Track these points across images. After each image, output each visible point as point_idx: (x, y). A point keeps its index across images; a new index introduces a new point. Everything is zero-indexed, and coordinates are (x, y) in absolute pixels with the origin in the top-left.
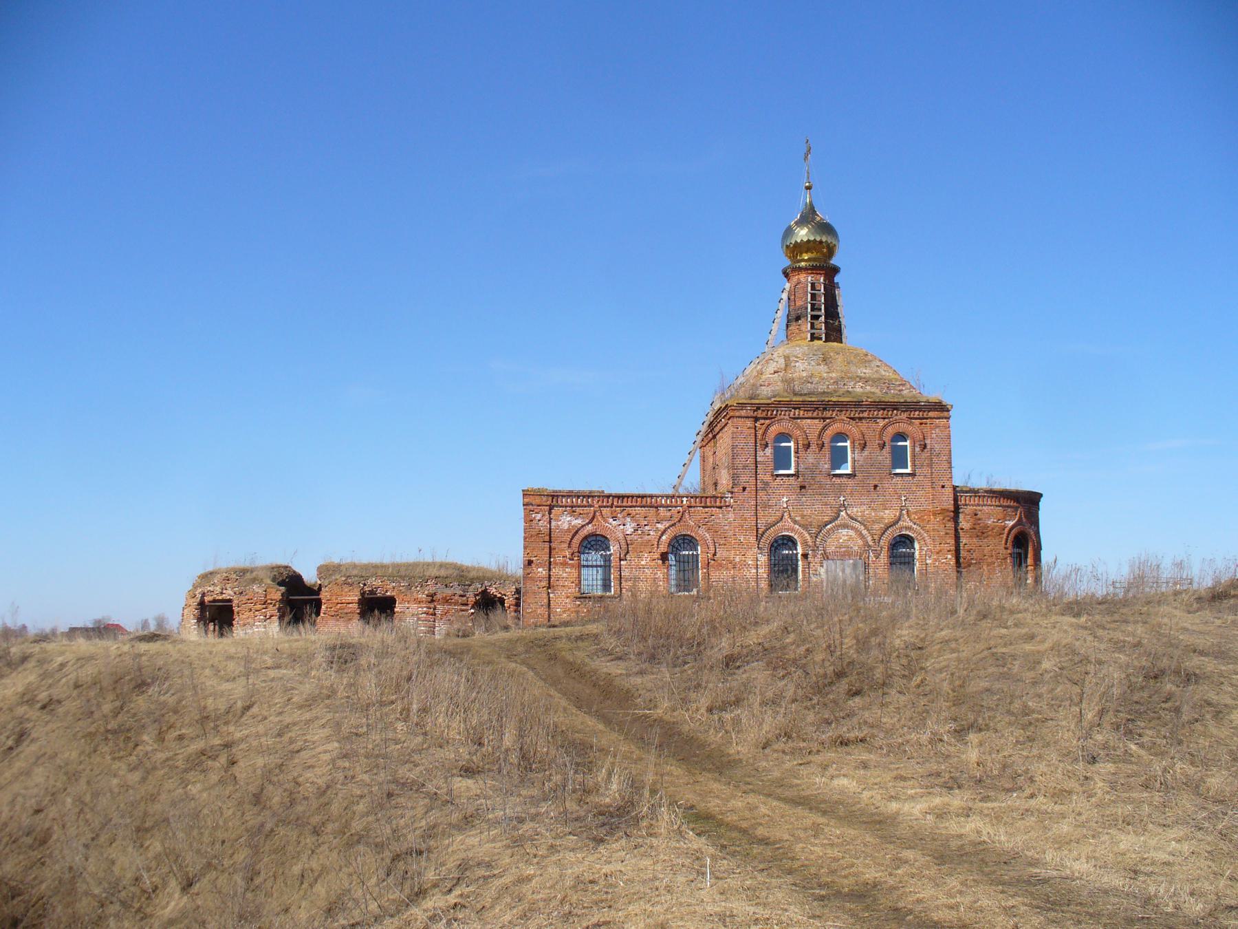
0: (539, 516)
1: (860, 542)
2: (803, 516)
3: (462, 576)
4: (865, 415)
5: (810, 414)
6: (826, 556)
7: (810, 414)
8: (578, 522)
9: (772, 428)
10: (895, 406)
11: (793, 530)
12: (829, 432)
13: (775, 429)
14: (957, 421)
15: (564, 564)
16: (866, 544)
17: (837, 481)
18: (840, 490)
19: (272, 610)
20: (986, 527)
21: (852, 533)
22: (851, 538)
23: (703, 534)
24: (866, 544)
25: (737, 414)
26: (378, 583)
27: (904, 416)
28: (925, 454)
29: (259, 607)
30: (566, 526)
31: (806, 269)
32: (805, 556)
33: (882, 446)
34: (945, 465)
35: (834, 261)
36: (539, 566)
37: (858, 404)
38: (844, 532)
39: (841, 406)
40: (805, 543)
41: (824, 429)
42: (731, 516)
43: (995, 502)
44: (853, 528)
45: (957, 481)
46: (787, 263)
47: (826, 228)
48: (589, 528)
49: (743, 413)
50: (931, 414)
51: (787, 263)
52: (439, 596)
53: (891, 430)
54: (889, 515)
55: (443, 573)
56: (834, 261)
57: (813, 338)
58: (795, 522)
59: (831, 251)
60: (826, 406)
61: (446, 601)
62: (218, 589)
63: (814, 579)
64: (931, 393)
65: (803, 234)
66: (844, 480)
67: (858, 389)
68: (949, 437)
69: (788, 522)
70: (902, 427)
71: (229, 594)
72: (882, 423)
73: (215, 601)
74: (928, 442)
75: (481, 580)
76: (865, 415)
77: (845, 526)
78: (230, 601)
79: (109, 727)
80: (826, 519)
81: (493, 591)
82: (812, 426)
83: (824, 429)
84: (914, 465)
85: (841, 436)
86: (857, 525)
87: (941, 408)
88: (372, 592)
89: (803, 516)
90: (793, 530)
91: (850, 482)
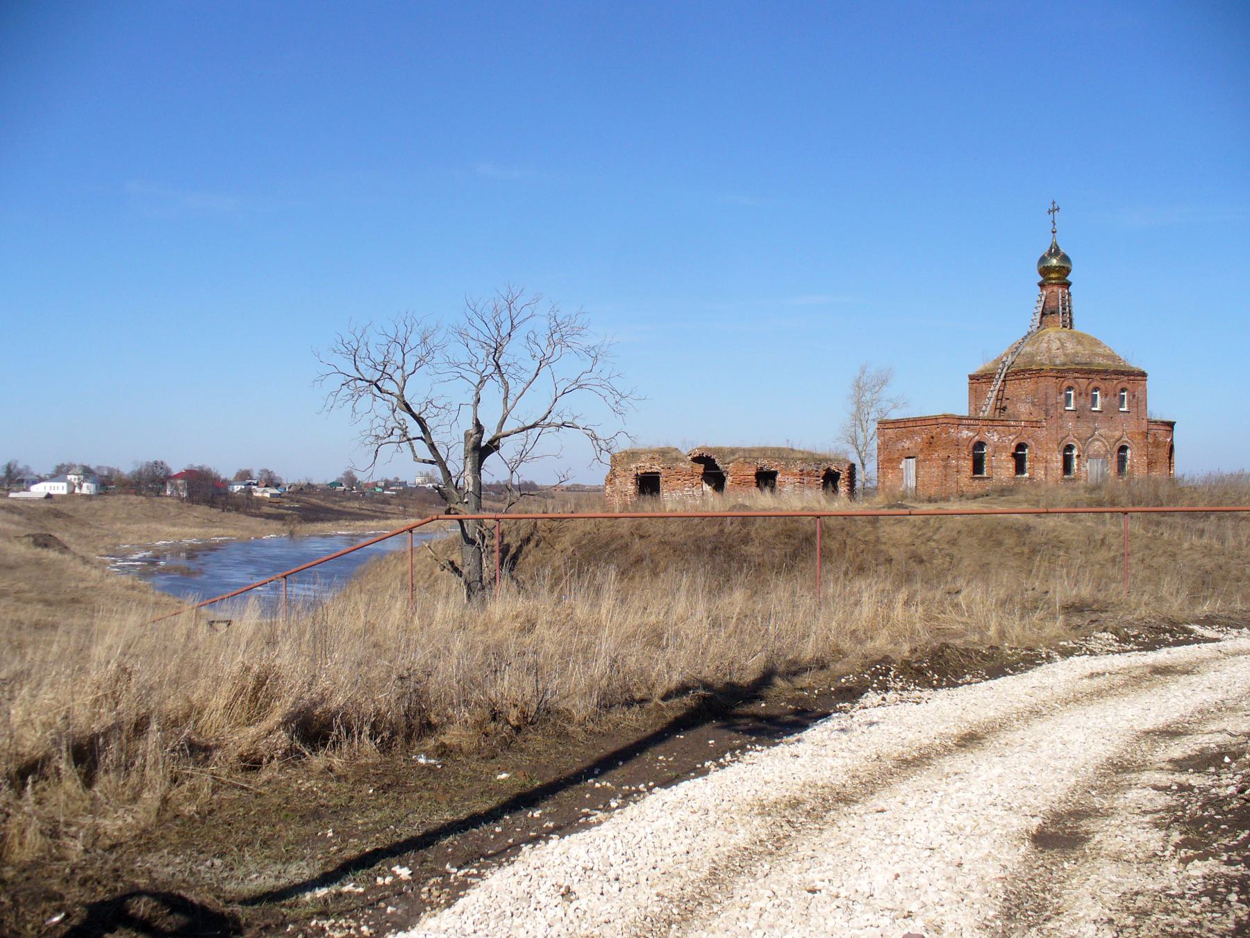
0: (952, 430)
1: (1104, 449)
2: (1078, 434)
3: (819, 460)
4: (1108, 377)
5: (1082, 376)
6: (1089, 457)
7: (1082, 376)
8: (971, 434)
9: (1065, 383)
10: (1123, 373)
11: (1073, 441)
12: (1091, 387)
13: (1066, 384)
14: (1150, 383)
15: (965, 458)
16: (1107, 450)
17: (1095, 414)
18: (1095, 419)
19: (697, 479)
20: (1159, 442)
21: (1100, 443)
22: (1100, 447)
23: (1030, 442)
24: (1107, 450)
25: (1049, 374)
26: (766, 462)
27: (1126, 378)
28: (1135, 400)
29: (686, 478)
30: (965, 437)
31: (1055, 284)
32: (1078, 456)
33: (1115, 395)
34: (1144, 407)
35: (1069, 278)
36: (953, 459)
37: (1106, 371)
38: (1097, 443)
39: (1098, 372)
40: (1079, 449)
41: (1089, 384)
42: (1045, 433)
43: (1163, 428)
44: (1101, 441)
45: (1148, 417)
46: (1040, 279)
47: (1065, 258)
48: (977, 438)
49: (1051, 374)
50: (1139, 378)
51: (1040, 279)
52: (805, 472)
53: (1119, 387)
54: (1117, 434)
55: (805, 456)
56: (1069, 278)
57: (1064, 326)
58: (1075, 437)
59: (1068, 271)
60: (1091, 372)
61: (808, 474)
62: (648, 465)
63: (477, 455)
64: (1136, 364)
65: (1054, 262)
66: (1097, 414)
67: (1100, 360)
68: (1146, 391)
69: (1125, 439)
70: (1124, 385)
71: (656, 468)
72: (1115, 382)
73: (646, 473)
74: (1136, 393)
75: (826, 460)
76: (1108, 377)
77: (1098, 440)
78: (657, 473)
79: (981, 536)
80: (1089, 435)
81: (833, 468)
82: (1083, 382)
83: (1089, 384)
84: (1129, 407)
85: (1096, 389)
86: (1103, 439)
87: (1144, 375)
88: (761, 468)
89: (1078, 434)
90: (1073, 441)
91: (1100, 415)
